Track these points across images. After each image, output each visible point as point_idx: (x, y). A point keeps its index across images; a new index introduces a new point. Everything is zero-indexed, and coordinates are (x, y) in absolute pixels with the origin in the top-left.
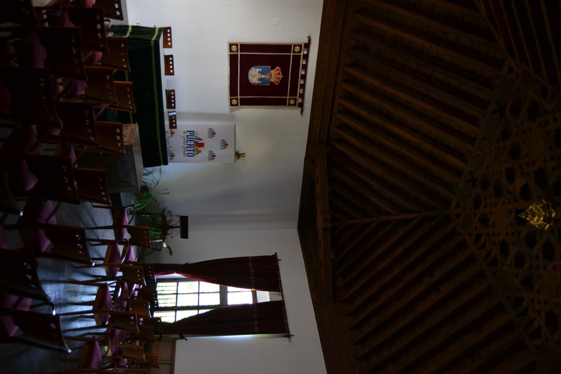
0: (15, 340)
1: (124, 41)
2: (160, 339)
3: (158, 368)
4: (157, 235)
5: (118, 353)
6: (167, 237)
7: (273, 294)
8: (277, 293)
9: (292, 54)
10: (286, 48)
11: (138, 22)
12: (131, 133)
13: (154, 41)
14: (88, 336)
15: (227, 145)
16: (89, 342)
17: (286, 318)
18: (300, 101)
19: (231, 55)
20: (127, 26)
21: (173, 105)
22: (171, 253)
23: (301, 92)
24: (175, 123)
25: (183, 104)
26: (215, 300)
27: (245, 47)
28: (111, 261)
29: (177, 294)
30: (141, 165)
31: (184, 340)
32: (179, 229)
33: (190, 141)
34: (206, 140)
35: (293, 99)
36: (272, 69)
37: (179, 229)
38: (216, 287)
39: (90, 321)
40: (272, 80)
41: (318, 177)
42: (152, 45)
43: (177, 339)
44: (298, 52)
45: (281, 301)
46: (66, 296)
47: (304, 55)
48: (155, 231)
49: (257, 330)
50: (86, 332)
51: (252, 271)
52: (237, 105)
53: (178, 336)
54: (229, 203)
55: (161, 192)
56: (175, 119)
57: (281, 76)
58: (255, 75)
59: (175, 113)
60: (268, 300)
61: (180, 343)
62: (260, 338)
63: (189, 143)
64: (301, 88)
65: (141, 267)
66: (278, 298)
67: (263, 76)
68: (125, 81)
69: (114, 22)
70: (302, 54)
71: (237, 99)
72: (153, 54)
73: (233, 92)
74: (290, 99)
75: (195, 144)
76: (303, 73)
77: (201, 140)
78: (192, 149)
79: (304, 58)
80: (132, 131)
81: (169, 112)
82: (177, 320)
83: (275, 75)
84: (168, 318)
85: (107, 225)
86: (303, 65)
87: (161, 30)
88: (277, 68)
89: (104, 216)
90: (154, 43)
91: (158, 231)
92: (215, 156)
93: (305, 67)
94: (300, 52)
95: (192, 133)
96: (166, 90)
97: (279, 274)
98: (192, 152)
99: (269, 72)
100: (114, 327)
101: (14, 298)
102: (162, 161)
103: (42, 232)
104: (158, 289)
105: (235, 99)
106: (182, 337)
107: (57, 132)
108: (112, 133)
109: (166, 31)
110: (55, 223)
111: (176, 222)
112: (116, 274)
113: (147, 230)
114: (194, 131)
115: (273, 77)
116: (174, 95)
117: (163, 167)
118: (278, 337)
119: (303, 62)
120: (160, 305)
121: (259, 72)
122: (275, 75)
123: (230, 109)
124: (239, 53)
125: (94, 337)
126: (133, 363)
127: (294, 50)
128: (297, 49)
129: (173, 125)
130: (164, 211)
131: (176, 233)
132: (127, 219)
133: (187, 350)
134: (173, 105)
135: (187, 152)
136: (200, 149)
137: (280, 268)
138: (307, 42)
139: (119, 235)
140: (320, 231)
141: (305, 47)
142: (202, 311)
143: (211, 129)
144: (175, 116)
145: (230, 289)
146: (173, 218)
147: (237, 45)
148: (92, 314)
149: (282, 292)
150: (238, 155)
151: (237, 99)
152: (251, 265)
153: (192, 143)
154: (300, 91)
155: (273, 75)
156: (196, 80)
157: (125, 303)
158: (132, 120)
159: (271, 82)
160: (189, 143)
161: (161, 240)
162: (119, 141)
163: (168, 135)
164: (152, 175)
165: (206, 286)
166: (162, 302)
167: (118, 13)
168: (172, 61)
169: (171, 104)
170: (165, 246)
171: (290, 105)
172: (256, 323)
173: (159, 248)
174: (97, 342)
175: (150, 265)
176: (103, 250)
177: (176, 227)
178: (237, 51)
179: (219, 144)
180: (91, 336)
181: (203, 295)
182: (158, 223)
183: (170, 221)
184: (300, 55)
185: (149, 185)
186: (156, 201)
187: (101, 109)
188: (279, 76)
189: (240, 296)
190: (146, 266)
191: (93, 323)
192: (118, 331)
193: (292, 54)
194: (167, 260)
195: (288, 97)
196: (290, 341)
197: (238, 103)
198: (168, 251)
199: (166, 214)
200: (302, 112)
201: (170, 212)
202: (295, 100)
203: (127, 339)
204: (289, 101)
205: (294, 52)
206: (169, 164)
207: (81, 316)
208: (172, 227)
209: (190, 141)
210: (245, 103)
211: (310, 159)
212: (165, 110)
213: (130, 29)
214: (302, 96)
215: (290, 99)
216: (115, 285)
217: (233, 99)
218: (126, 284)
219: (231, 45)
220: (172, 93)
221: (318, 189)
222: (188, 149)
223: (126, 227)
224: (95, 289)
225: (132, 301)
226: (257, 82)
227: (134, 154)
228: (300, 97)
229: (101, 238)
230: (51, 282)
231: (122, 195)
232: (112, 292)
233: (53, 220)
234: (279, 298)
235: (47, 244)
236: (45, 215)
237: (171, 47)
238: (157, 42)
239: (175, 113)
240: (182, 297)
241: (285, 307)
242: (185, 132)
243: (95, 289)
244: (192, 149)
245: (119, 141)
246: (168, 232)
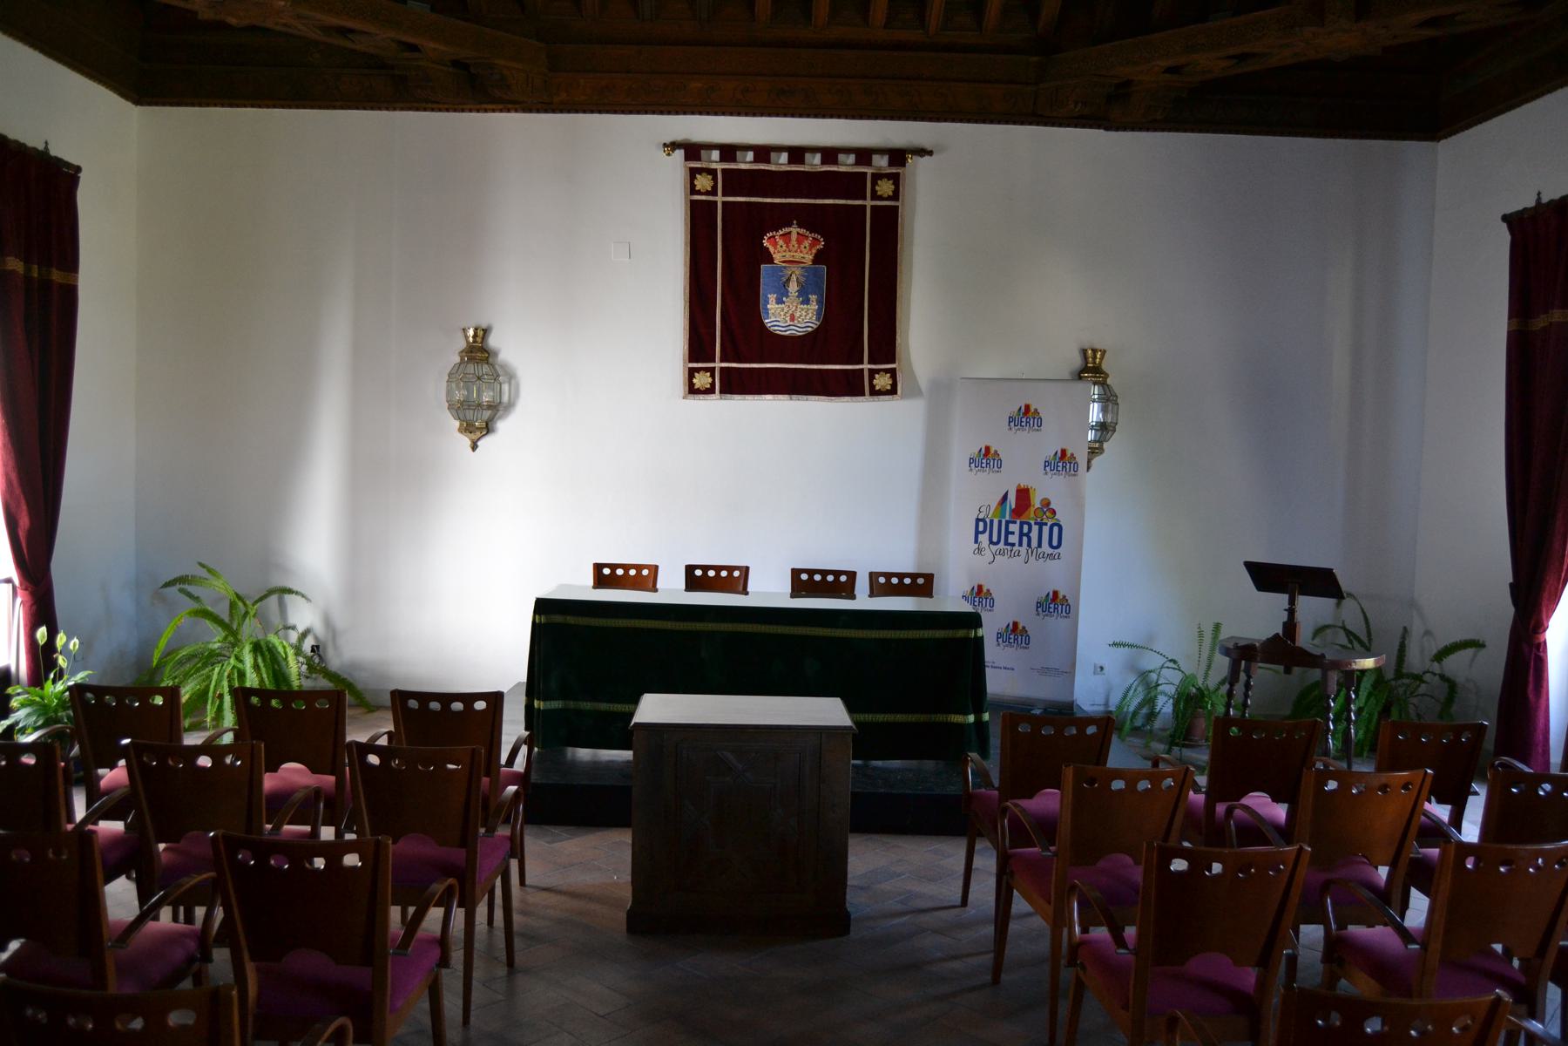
9: (720, 199)
10: (700, 217)
18: (881, 162)
21: (843, 578)
27: (698, 348)
33: (1008, 533)
34: (1006, 482)
35: (874, 184)
36: (770, 260)
40: (809, 258)
47: (723, 159)
52: (893, 372)
57: (794, 230)
58: (789, 314)
63: (1013, 539)
64: (835, 162)
67: (793, 288)
71: (872, 373)
72: (571, 620)
73: (849, 386)
75: (1022, 518)
77: (1005, 498)
78: (1035, 528)
79: (734, 160)
83: (791, 251)
86: (756, 160)
88: (765, 243)
93: (763, 153)
94: (713, 172)
98: (1046, 529)
99: (781, 269)
105: (872, 378)
114: (978, 520)
115: (798, 256)
119: (746, 162)
121: (779, 301)
122: (791, 251)
124: (718, 365)
127: (707, 193)
134: (843, 578)
136: (1036, 502)
138: (679, 154)
141: (699, 159)
147: (692, 373)
150: (1090, 369)
151: (872, 373)
153: (1014, 528)
154: (847, 164)
159: (816, 261)
160: (1013, 539)
167: (1091, 730)
169: (841, 584)
177: (1291, 612)
179: (1024, 436)
184: (724, 171)
188: (794, 237)
193: (720, 199)
194: (1489, 668)
195: (869, 203)
200: (922, 152)
202: (877, 177)
205: (714, 192)
208: (1290, 627)
210: (886, 348)
211: (1107, 110)
214: (864, 155)
215: (875, 196)
219: (693, 390)
220: (882, 580)
222: (1034, 543)
226: (814, 306)
228: (869, 163)
242: (980, 550)
244: (1035, 528)
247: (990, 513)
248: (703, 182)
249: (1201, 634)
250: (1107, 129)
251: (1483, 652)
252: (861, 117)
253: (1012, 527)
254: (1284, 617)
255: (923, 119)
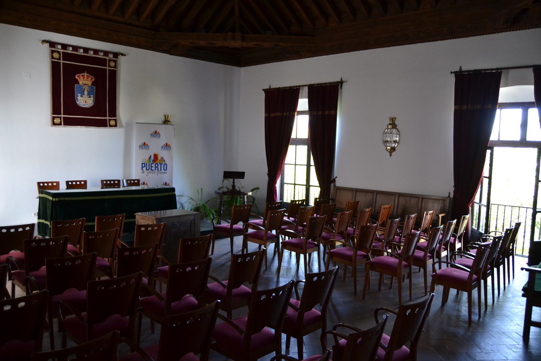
0: (324, 311)
1: (55, 225)
2: (333, 200)
3: (358, 201)
4: (240, 201)
5: (342, 234)
6: (242, 191)
7: (302, 95)
8: (301, 91)
9: (62, 61)
10: (55, 67)
11: (33, 214)
12: (143, 219)
13: (53, 198)
14: (326, 260)
15: (156, 131)
16: (331, 256)
17: (325, 83)
18: (111, 56)
19: (64, 125)
20: (39, 223)
22: (258, 188)
23: (102, 54)
24: (134, 180)
25: (115, 173)
26: (303, 150)
27: (56, 110)
28: (262, 238)
29: (295, 184)
30: (174, 210)
31: (336, 179)
32: (236, 180)
33: (152, 167)
35: (109, 63)
36: (78, 83)
37: (236, 180)
38: (291, 148)
39: (313, 258)
40: (90, 83)
41: (190, 43)
42: (57, 199)
43: (335, 185)
44: (60, 55)
45: (309, 88)
46: (291, 277)
47: (62, 48)
48: (236, 202)
49: (333, 112)
50: (322, 262)
51: (279, 114)
53: (332, 185)
54: (212, 132)
55: (200, 197)
56: (130, 180)
57: (86, 74)
58: (85, 101)
59: (125, 180)
60: (307, 100)
61: (339, 183)
62: (341, 109)
63: (153, 168)
65: (269, 212)
66: (305, 90)
67: (86, 92)
68: (94, 225)
69: (36, 234)
70: (61, 51)
71: (110, 120)
72: (66, 199)
73: (102, 124)
74: (109, 66)
75: (155, 162)
76: (82, 51)
77: (150, 157)
78: (159, 165)
79: (66, 49)
80: (143, 219)
81: (124, 186)
82: (318, 185)
83: (84, 81)
84: (315, 193)
85: (230, 243)
86: (73, 50)
87: (40, 192)
88: (76, 77)
89: (221, 248)
90: (55, 198)
91: (237, 200)
92: (167, 144)
93: (75, 48)
94: (59, 52)
95: (143, 165)
96: (102, 188)
97: (283, 88)
100: (320, 237)
101: (290, 311)
102: (171, 193)
103: (235, 291)
104: (289, 202)
105: (109, 122)
106: (334, 181)
107: (145, 280)
108: (145, 234)
109: (42, 187)
110: (227, 281)
111: (228, 183)
112: (274, 235)
113: (236, 207)
116: (106, 181)
117: (177, 193)
118: (341, 92)
119: (70, 50)
120: (304, 198)
121: (82, 96)
122: (84, 81)
123: (120, 127)
124: (62, 116)
125: (327, 253)
126: (352, 223)
127: (57, 59)
128: (56, 55)
129: (137, 183)
130: (218, 193)
131: (240, 184)
132: (225, 224)
133: (345, 176)
134: (116, 182)
135: (163, 170)
136: (159, 158)
137: (277, 86)
138: (47, 45)
139: (239, 232)
140: (244, 44)
141: (54, 47)
142: (312, 163)
143: (140, 146)
144: (127, 181)
145: (293, 136)
146: (225, 186)
147: (54, 118)
148: (307, 254)
149: (300, 86)
150: (166, 121)
151: (110, 120)
152: (273, 115)
154: (101, 55)
155: (84, 82)
156: (92, 159)
157: (300, 228)
158: (132, 220)
159: (92, 85)
161: (246, 197)
162: (153, 228)
163: (145, 187)
164: (184, 204)
165: (289, 158)
166: (301, 196)
168: (72, 182)
169: (116, 183)
170: (250, 194)
171: (115, 67)
172: (327, 112)
173: (253, 199)
174: (331, 251)
175: (267, 205)
176: (253, 246)
177: (234, 183)
178: (60, 118)
180: (326, 255)
181: (297, 160)
182: (229, 199)
183: (228, 189)
184: (63, 52)
185: (193, 207)
186: (209, 200)
187: (122, 244)
188: (86, 76)
189: (301, 127)
190: (268, 209)
191: (315, 255)
192: (324, 234)
193: (62, 61)
194: (263, 192)
195: (108, 68)
196: (346, 82)
197: (114, 120)
198: (255, 191)
199: (221, 191)
200: (123, 55)
201: (219, 189)
202: (110, 60)
203: (331, 226)
204: (111, 67)
205: (59, 59)
206: (173, 187)
207: (308, 264)
208: (234, 186)
209: (152, 167)
210: (113, 113)
212: (121, 189)
213: (41, 221)
214: (106, 53)
215: (109, 66)
216: (283, 236)
217: (110, 124)
218: (283, 227)
219: (54, 124)
220: (105, 182)
221: (202, 43)
222: (159, 169)
223: (232, 226)
224: (286, 253)
225: (299, 222)
227: (165, 216)
228: (108, 56)
229: (241, 248)
230: (278, 282)
231: (203, 229)
232: (289, 239)
233: (225, 282)
234: (306, 89)
235: (245, 288)
236: (221, 289)
237: (58, 183)
238: (54, 195)
239: (125, 180)
240: (298, 181)
241: (314, 84)
242: (143, 172)
243: (286, 253)
244: (159, 165)
245: (153, 228)
246: (238, 190)
247: (146, 161)
248: (56, 55)
249: (198, 191)
250: (170, 54)
251: (259, 190)
252: (105, 41)
253: (153, 165)
254: (232, 184)
255: (122, 45)
